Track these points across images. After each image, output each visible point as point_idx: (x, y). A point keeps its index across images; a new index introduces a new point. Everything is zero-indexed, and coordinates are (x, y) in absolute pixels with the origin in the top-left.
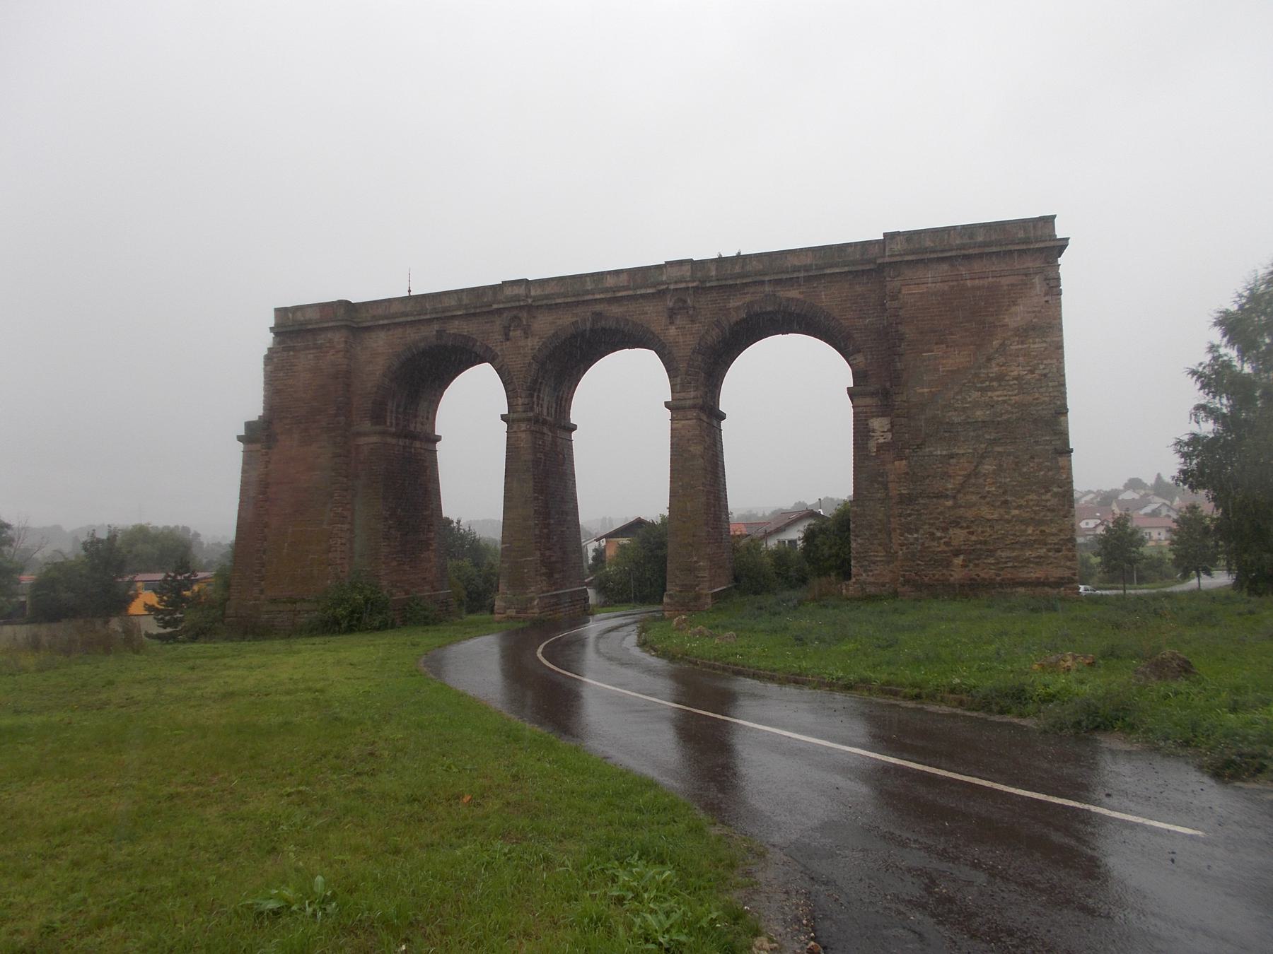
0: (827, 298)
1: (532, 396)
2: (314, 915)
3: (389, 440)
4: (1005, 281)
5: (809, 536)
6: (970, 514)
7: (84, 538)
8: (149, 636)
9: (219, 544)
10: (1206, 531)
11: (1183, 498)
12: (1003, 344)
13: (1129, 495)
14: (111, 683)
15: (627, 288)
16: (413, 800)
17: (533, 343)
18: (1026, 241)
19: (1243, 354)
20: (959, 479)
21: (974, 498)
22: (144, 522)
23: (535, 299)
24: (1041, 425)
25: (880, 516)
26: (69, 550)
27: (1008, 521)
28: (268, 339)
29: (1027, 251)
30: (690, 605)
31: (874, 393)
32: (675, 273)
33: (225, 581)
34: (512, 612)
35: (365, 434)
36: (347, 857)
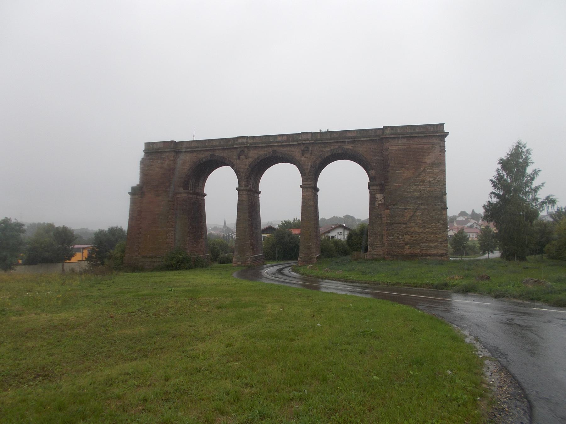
0: (361, 149)
1: (248, 181)
3: (190, 196)
5: (350, 236)
6: (412, 230)
10: (493, 237)
11: (483, 224)
12: (424, 169)
13: (461, 218)
15: (285, 142)
17: (250, 161)
19: (508, 174)
20: (408, 217)
21: (413, 224)
23: (250, 144)
25: (379, 230)
27: (425, 233)
29: (434, 135)
30: (308, 261)
32: (305, 137)
34: (239, 263)
35: (180, 193)
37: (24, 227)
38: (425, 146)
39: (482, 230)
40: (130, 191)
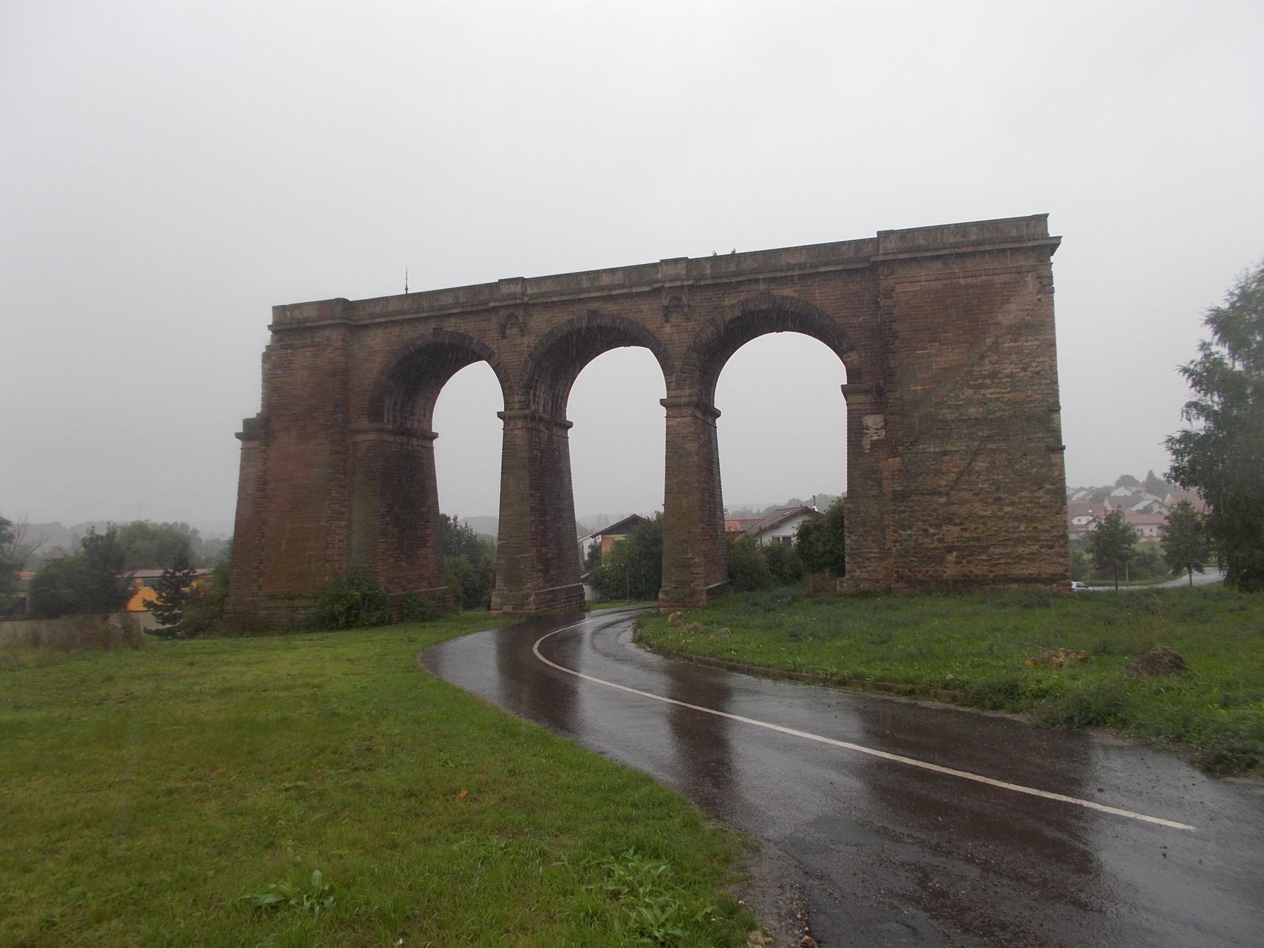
0: (821, 297)
2: (312, 909)
3: (391, 438)
4: (998, 279)
5: (804, 533)
6: (963, 511)
7: (84, 535)
8: (148, 632)
9: (217, 541)
10: (1198, 527)
11: (1174, 495)
12: (995, 342)
13: (1121, 492)
14: (110, 678)
15: (622, 286)
16: (410, 795)
17: (529, 341)
18: (1019, 239)
19: (1234, 351)
20: (953, 476)
21: (967, 495)
22: (143, 518)
23: (531, 297)
24: (1033, 422)
25: (874, 513)
26: (69, 546)
27: (1001, 518)
28: (266, 337)
29: (1020, 249)
30: (685, 601)
31: (867, 391)
32: (670, 271)
33: (223, 577)
34: (508, 608)
36: (344, 851)
37: (10, 529)
38: (998, 279)
39: (1173, 518)
40: (241, 430)
